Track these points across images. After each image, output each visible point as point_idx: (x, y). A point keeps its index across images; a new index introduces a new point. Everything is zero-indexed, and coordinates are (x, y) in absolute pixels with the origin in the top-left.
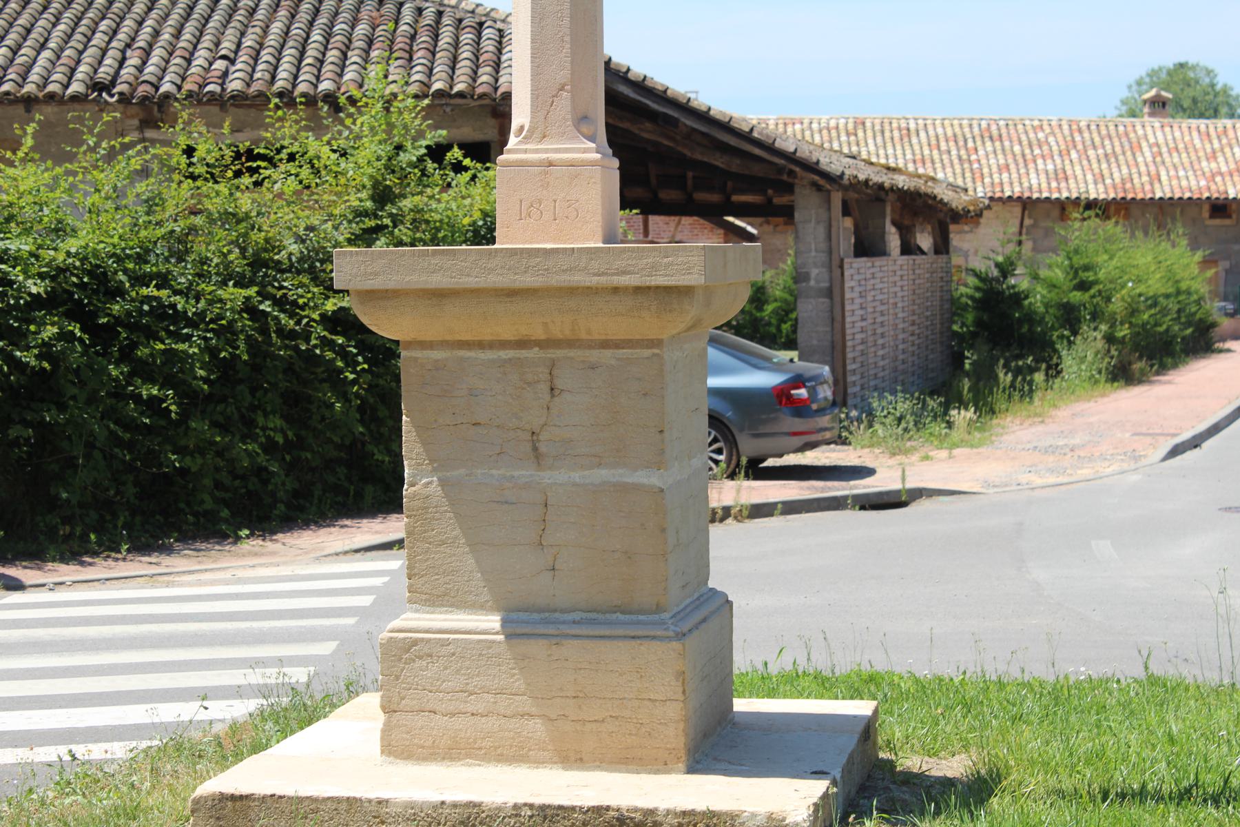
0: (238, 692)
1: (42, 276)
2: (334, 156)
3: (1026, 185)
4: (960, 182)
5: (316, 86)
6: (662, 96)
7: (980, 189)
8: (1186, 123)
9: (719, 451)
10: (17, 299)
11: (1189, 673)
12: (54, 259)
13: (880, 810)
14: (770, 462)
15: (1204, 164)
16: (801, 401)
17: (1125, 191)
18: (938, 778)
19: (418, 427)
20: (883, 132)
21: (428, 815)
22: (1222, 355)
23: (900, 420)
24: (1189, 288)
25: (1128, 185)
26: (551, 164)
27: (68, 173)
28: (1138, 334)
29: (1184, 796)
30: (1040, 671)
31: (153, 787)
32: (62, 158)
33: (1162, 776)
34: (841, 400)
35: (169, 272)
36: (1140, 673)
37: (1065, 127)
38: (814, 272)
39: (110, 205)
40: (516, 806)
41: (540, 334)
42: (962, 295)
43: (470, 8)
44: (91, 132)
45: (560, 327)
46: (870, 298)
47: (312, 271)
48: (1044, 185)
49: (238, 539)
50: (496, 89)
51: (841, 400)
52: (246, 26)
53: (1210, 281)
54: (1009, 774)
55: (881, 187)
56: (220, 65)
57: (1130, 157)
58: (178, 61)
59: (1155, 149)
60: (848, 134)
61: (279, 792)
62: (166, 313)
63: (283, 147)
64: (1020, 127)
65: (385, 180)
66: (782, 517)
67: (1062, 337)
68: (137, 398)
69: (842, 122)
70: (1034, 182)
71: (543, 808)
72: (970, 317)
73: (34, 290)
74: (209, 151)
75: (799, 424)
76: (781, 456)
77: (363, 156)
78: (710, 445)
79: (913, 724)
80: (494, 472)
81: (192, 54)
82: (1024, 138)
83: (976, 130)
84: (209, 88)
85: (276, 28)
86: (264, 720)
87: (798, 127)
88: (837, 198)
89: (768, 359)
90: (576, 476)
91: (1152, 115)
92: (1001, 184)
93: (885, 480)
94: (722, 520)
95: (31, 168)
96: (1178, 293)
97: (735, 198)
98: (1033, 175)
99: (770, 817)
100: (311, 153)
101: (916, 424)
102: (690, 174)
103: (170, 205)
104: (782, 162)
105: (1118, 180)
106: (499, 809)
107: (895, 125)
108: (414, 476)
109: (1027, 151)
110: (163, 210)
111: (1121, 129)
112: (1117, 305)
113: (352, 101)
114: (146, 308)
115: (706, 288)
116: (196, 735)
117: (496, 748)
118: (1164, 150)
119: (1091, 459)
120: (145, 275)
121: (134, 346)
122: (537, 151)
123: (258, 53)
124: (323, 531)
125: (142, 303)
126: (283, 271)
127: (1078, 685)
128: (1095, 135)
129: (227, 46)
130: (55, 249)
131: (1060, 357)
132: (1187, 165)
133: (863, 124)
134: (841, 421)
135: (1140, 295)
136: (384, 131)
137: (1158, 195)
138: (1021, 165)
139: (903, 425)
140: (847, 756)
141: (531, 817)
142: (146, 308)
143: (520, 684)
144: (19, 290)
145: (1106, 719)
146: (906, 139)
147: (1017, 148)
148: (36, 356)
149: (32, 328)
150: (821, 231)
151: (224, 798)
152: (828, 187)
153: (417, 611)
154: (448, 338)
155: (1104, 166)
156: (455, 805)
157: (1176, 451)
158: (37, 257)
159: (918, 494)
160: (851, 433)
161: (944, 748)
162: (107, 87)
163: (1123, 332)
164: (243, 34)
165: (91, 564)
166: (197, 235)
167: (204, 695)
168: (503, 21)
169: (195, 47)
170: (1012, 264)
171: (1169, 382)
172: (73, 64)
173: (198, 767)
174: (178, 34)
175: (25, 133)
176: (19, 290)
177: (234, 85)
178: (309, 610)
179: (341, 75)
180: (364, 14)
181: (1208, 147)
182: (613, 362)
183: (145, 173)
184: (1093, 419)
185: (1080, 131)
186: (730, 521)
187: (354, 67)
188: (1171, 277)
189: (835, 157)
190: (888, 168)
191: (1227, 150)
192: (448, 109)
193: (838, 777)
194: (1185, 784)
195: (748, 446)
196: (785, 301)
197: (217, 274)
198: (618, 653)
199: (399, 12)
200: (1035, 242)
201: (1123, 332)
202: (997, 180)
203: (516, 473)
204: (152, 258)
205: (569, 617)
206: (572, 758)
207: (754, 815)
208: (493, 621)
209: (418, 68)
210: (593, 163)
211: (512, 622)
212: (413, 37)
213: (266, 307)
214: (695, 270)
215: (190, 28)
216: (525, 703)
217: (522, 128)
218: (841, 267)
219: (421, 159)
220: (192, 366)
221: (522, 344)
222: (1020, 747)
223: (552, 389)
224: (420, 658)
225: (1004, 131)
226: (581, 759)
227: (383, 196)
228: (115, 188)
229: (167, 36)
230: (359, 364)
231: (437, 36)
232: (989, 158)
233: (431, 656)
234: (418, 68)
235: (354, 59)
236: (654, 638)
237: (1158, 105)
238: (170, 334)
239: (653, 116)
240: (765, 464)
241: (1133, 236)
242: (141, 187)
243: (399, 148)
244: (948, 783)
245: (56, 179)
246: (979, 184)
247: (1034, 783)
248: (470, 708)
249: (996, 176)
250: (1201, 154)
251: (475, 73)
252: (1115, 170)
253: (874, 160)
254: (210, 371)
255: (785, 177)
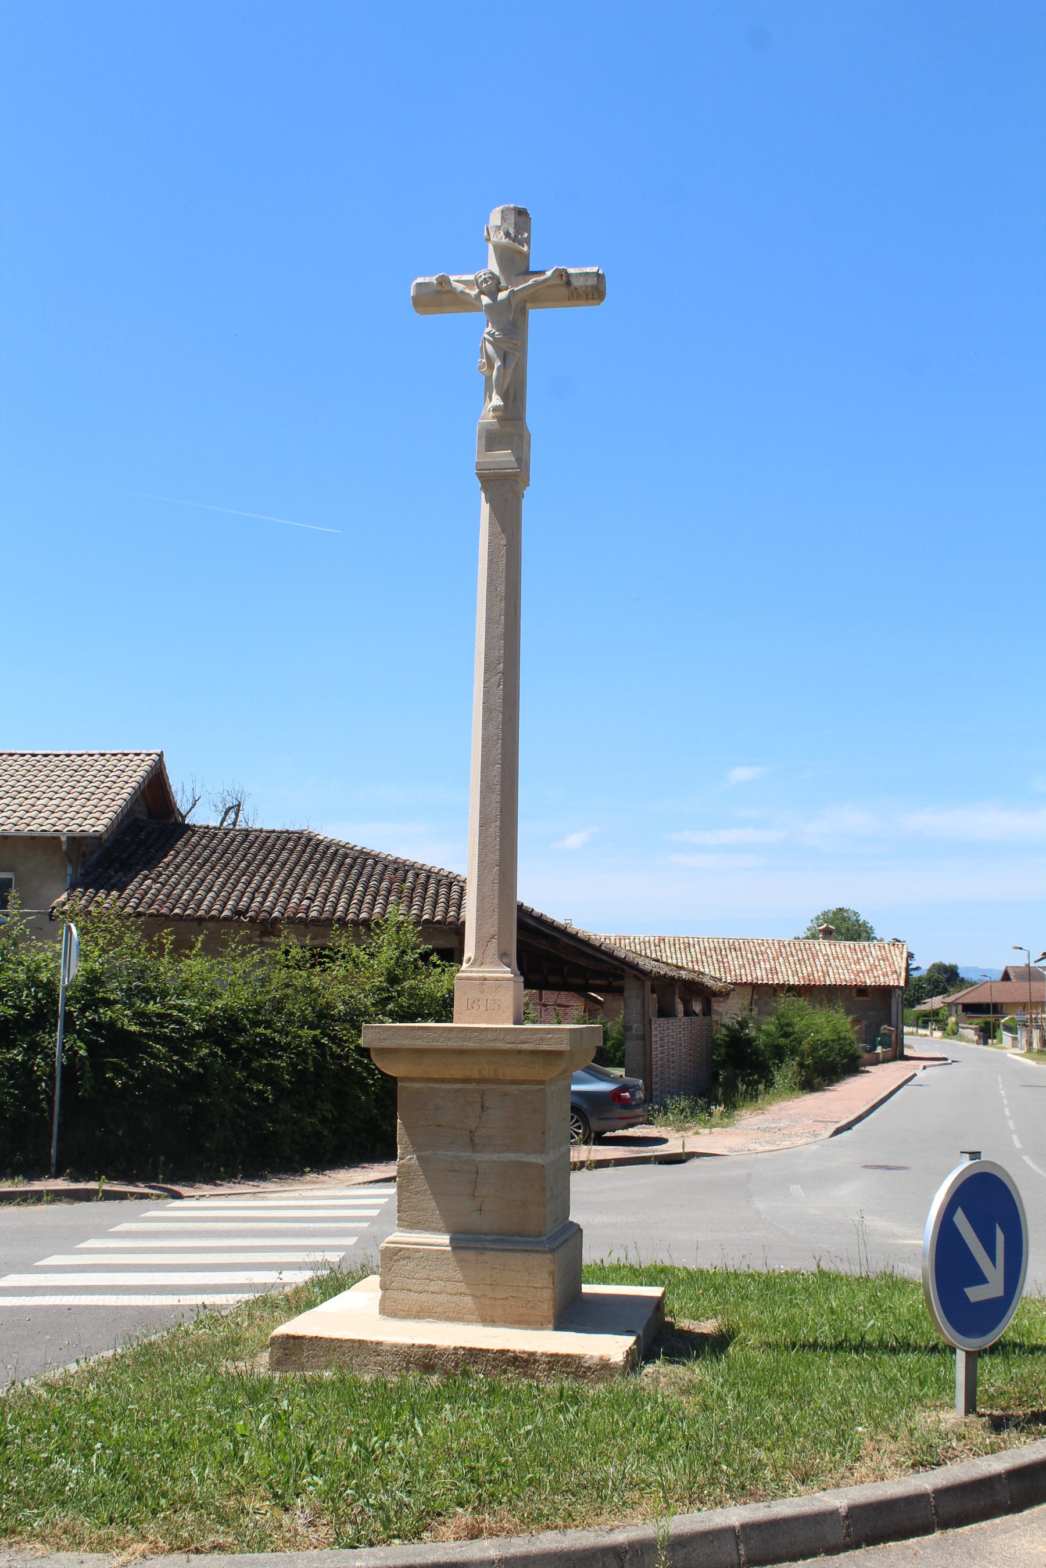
0: (299, 1267)
1: (202, 1020)
2: (367, 957)
3: (754, 976)
4: (718, 975)
5: (358, 916)
6: (551, 925)
7: (729, 978)
8: (842, 943)
9: (579, 1128)
10: (187, 1033)
11: (844, 1268)
12: (209, 1011)
13: (665, 1354)
14: (608, 1134)
15: (853, 966)
16: (625, 1099)
17: (809, 980)
18: (699, 1334)
19: (407, 1127)
20: (675, 945)
21: (405, 1352)
22: (864, 1074)
23: (682, 1111)
24: (846, 1036)
25: (811, 977)
26: (485, 979)
27: (219, 963)
28: (817, 1062)
29: (838, 1347)
30: (758, 1266)
31: (249, 1325)
32: (216, 954)
33: (825, 1334)
34: (649, 1099)
35: (272, 1020)
36: (815, 1270)
37: (776, 944)
38: (635, 1026)
39: (241, 981)
40: (455, 1348)
41: (475, 1075)
42: (718, 1039)
43: (445, 874)
44: (233, 941)
45: (488, 1072)
46: (666, 1041)
47: (352, 1021)
48: (765, 976)
49: (303, 1173)
50: (458, 919)
51: (649, 1099)
52: (322, 881)
53: (857, 1032)
54: (739, 1332)
55: (673, 978)
56: (306, 902)
57: (812, 962)
58: (283, 899)
59: (826, 958)
60: (655, 946)
61: (320, 1335)
62: (269, 1042)
63: (339, 951)
64: (751, 943)
65: (395, 970)
66: (614, 1168)
67: (774, 1064)
68: (251, 1090)
69: (652, 938)
70: (759, 974)
71: (471, 1350)
72: (723, 1051)
73: (197, 1028)
74: (298, 953)
75: (625, 1113)
76: (614, 1131)
77: (383, 957)
78: (574, 1124)
79: (685, 1300)
80: (448, 1153)
81: (291, 896)
82: (753, 949)
83: (727, 945)
84: (299, 915)
85: (338, 882)
86: (314, 1286)
87: (627, 941)
88: (648, 985)
89: (608, 1075)
90: (495, 1157)
91: (823, 938)
92: (741, 975)
93: (672, 1147)
94: (579, 1169)
95: (199, 960)
96: (839, 1039)
97: (591, 982)
98: (758, 971)
99: (601, 1359)
100: (354, 955)
101: (691, 1114)
102: (566, 968)
103: (275, 981)
104: (617, 963)
105: (805, 974)
106: (446, 1349)
107: (681, 941)
108: (403, 1154)
109: (755, 957)
110: (270, 985)
111: (807, 945)
112: (805, 1046)
113: (377, 924)
114: (258, 1039)
115: (571, 1052)
116: (274, 1293)
117: (445, 1313)
118: (831, 958)
119: (790, 1136)
120: (259, 1021)
121: (250, 1061)
122: (478, 972)
123: (327, 896)
124: (352, 1170)
125: (256, 1037)
126: (335, 1021)
127: (780, 1276)
128: (793, 949)
129: (310, 892)
130: (209, 1005)
131: (773, 1076)
132: (843, 966)
133: (664, 940)
134: (649, 1111)
135: (818, 1040)
136: (396, 944)
137: (828, 983)
138: (752, 965)
139: (684, 1114)
140: (646, 1321)
141: (463, 1355)
142: (258, 1039)
143: (459, 1276)
144: (188, 1027)
145: (796, 1299)
146: (687, 949)
147: (749, 955)
148: (196, 1065)
149: (195, 1049)
150: (639, 1003)
151: (289, 1337)
152: (643, 978)
153: (402, 1231)
154: (425, 1076)
155: (798, 966)
156: (420, 1346)
157: (838, 1131)
158: (200, 1010)
159: (692, 1155)
160: (654, 1118)
161: (702, 1315)
162: (243, 913)
163: (809, 1061)
164: (319, 886)
165: (220, 1185)
166: (288, 999)
167: (281, 1267)
168: (464, 882)
169: (293, 892)
170: (746, 1022)
171: (834, 1090)
172: (225, 900)
173: (276, 1314)
174: (283, 885)
175: (197, 940)
176: (188, 1027)
177: (313, 914)
178: (342, 1217)
179: (372, 910)
180: (386, 876)
181: (855, 956)
182: (517, 1092)
183: (262, 963)
184: (790, 1112)
185: (784, 947)
186: (584, 1169)
187: (380, 905)
188: (835, 1030)
189: (647, 961)
190: (677, 967)
191: (865, 958)
192: (431, 930)
193: (641, 1334)
194: (839, 1339)
195: (595, 1125)
196: (618, 1039)
197: (298, 1021)
198: (515, 1260)
199: (406, 876)
200: (759, 1008)
201: (809, 1061)
202: (738, 973)
203: (461, 1154)
204: (263, 1011)
205: (489, 1238)
206: (488, 1319)
207: (592, 1357)
208: (445, 1239)
209: (415, 907)
210: (509, 979)
211: (456, 1239)
212: (413, 890)
213: (325, 1041)
214: (565, 1042)
215: (290, 882)
216: (462, 1287)
217: (470, 959)
218: (650, 1023)
219: (415, 960)
220: (282, 1072)
221: (466, 1080)
222: (745, 1314)
223: (482, 1107)
224: (403, 1259)
225: (742, 945)
226: (494, 1321)
227: (393, 979)
228: (244, 972)
229: (277, 886)
230: (376, 1075)
231: (427, 889)
232: (733, 960)
233: (409, 1258)
234: (415, 907)
235: (380, 901)
236: (537, 1251)
237: (827, 934)
238: (271, 1055)
239: (546, 936)
240: (605, 1135)
241: (814, 1007)
242: (259, 972)
243: (404, 952)
244: (704, 1337)
245: (212, 967)
246: (728, 975)
247: (753, 1339)
248: (431, 1289)
249: (737, 971)
250: (851, 960)
251: (447, 910)
252: (804, 968)
253: (669, 961)
254: (292, 1077)
255: (619, 972)
